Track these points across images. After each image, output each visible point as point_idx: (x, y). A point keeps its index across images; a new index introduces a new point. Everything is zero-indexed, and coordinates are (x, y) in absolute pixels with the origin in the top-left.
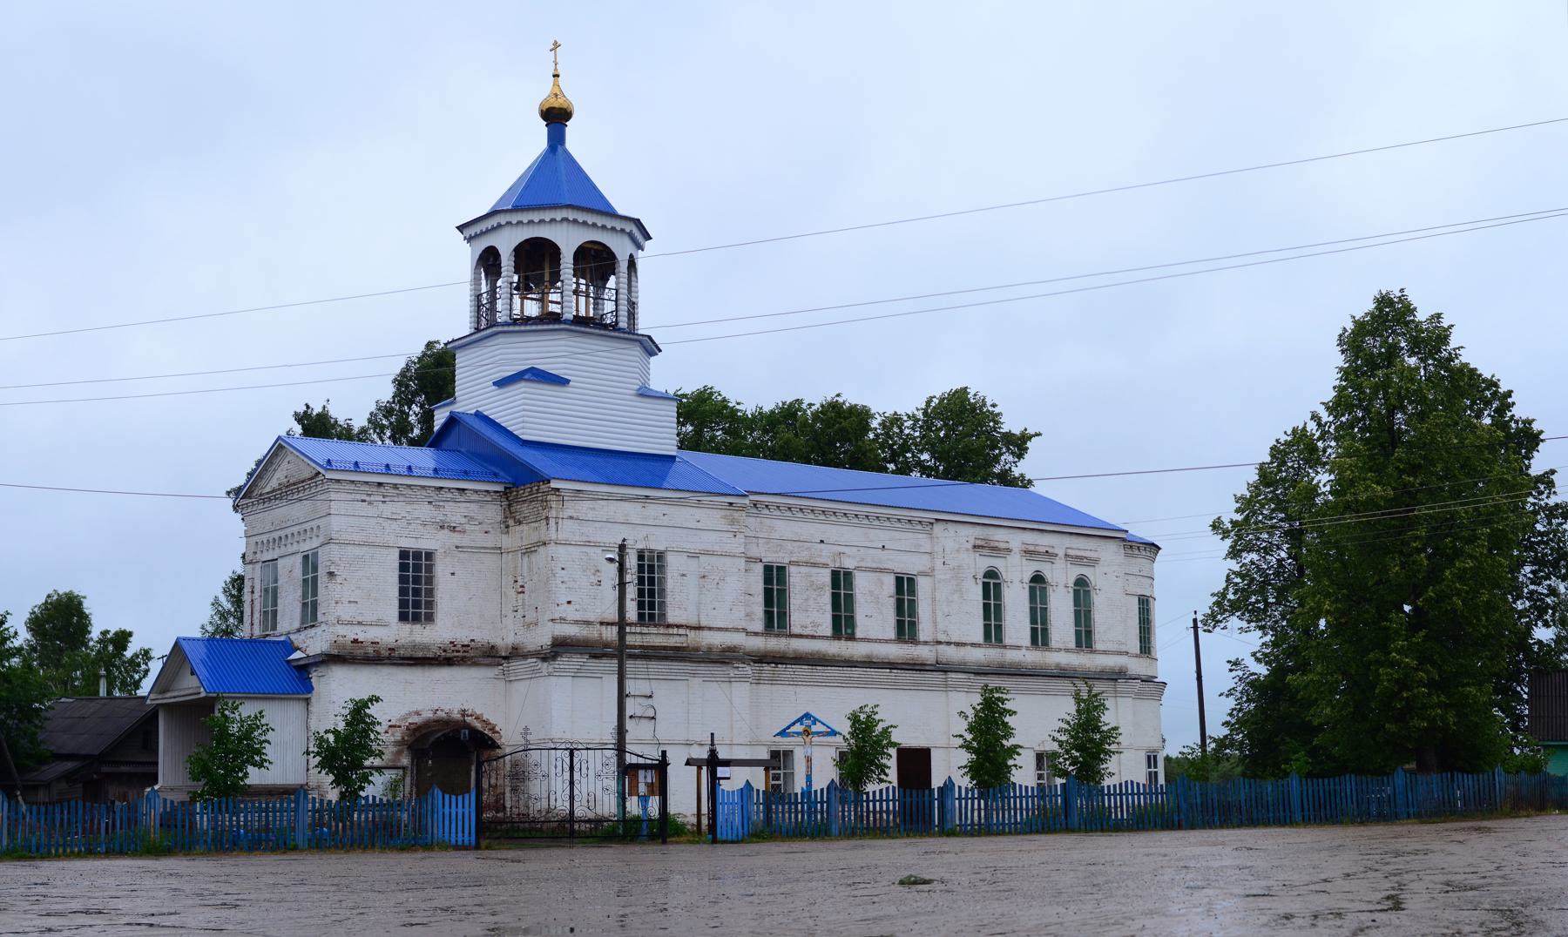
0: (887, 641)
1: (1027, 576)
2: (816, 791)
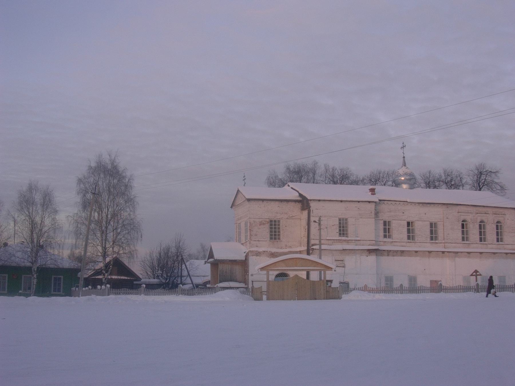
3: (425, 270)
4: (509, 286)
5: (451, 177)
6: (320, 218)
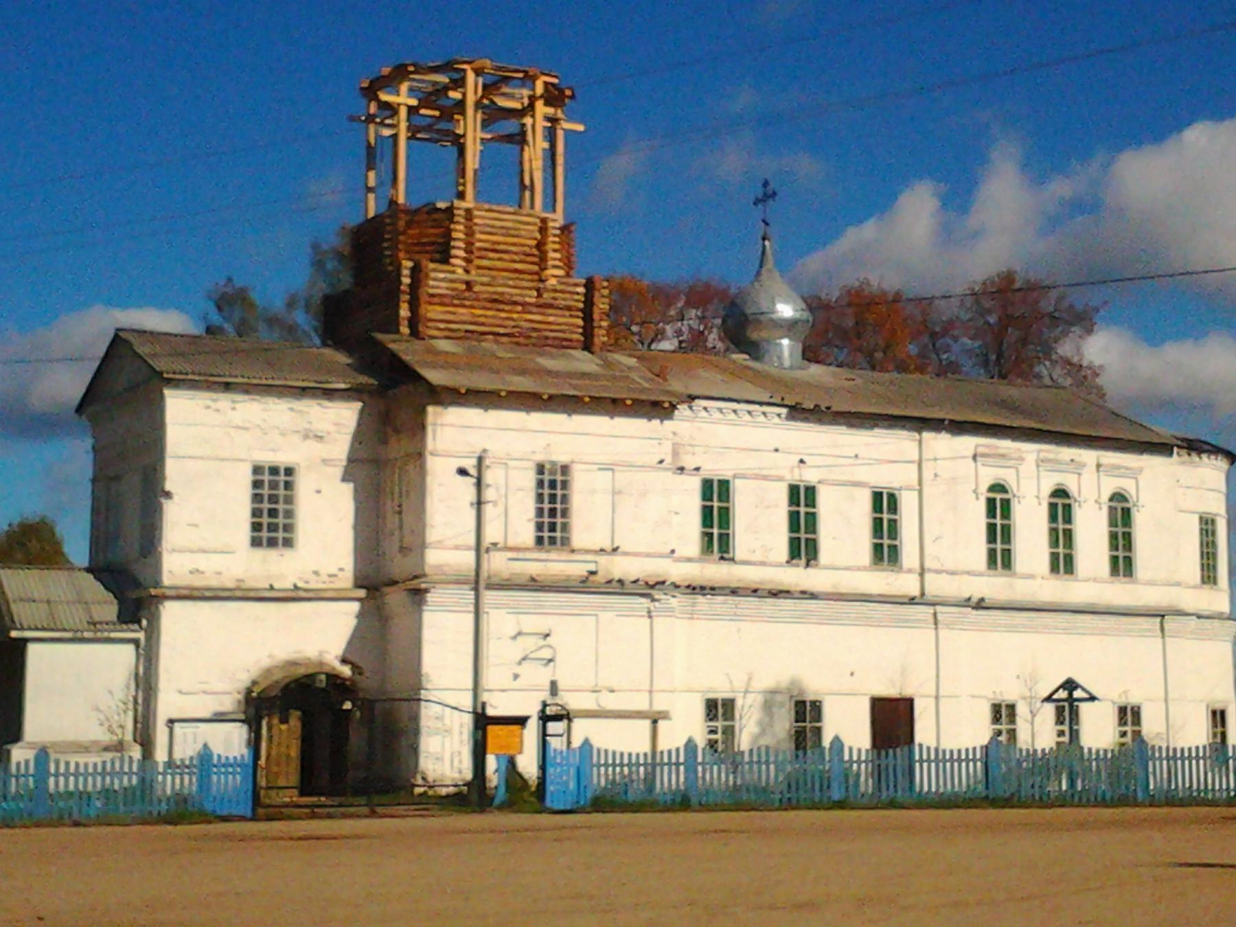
0: (859, 569)
1: (1047, 487)
2: (662, 753)
3: (852, 674)
4: (952, 752)
5: (546, 290)
6: (480, 460)
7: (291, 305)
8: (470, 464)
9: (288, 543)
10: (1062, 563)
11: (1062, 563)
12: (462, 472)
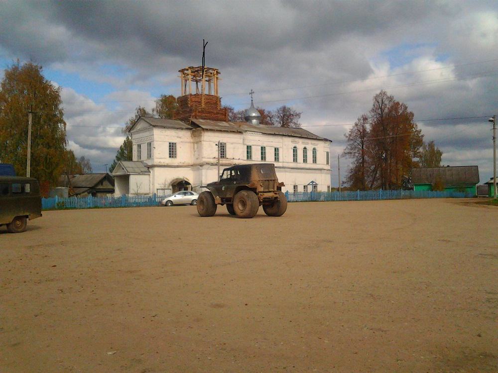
7: (153, 110)
8: (217, 144)
9: (176, 157)
10: (305, 161)
11: (305, 161)
12: (216, 145)
